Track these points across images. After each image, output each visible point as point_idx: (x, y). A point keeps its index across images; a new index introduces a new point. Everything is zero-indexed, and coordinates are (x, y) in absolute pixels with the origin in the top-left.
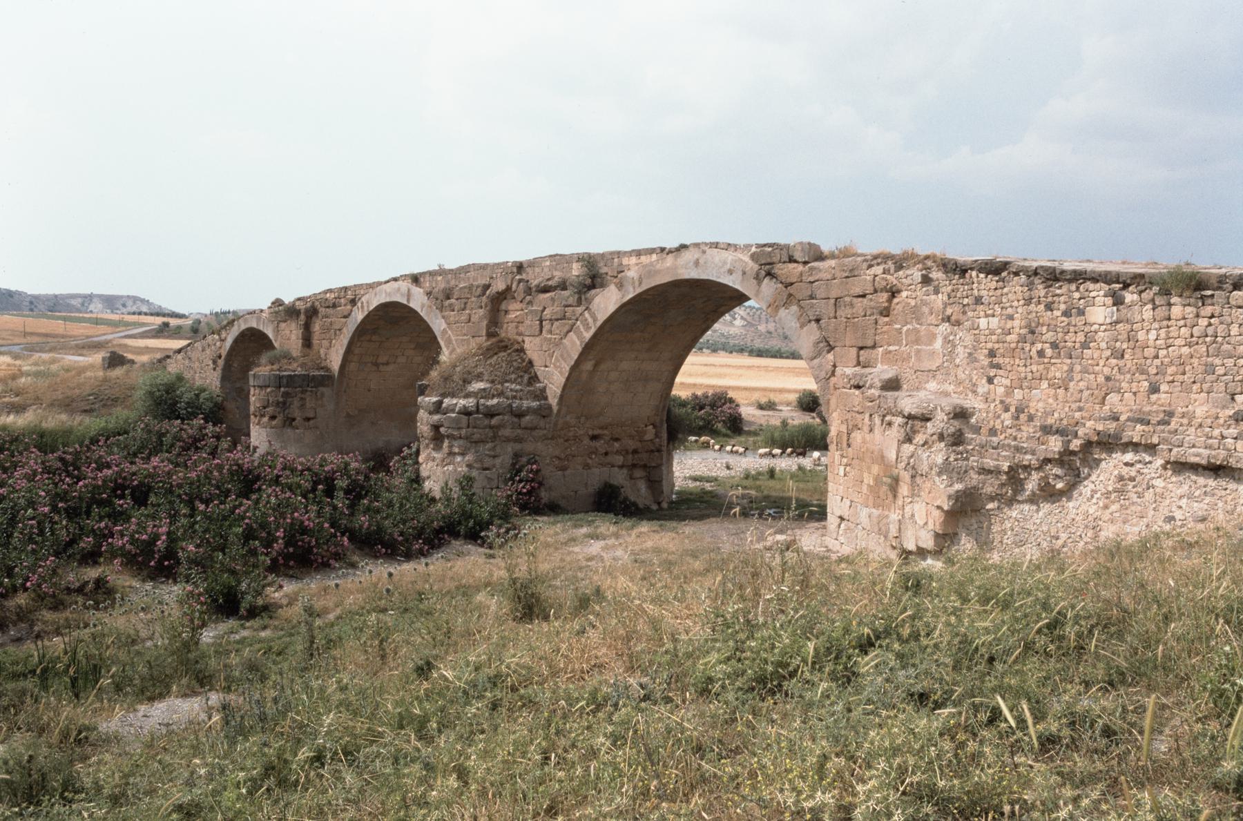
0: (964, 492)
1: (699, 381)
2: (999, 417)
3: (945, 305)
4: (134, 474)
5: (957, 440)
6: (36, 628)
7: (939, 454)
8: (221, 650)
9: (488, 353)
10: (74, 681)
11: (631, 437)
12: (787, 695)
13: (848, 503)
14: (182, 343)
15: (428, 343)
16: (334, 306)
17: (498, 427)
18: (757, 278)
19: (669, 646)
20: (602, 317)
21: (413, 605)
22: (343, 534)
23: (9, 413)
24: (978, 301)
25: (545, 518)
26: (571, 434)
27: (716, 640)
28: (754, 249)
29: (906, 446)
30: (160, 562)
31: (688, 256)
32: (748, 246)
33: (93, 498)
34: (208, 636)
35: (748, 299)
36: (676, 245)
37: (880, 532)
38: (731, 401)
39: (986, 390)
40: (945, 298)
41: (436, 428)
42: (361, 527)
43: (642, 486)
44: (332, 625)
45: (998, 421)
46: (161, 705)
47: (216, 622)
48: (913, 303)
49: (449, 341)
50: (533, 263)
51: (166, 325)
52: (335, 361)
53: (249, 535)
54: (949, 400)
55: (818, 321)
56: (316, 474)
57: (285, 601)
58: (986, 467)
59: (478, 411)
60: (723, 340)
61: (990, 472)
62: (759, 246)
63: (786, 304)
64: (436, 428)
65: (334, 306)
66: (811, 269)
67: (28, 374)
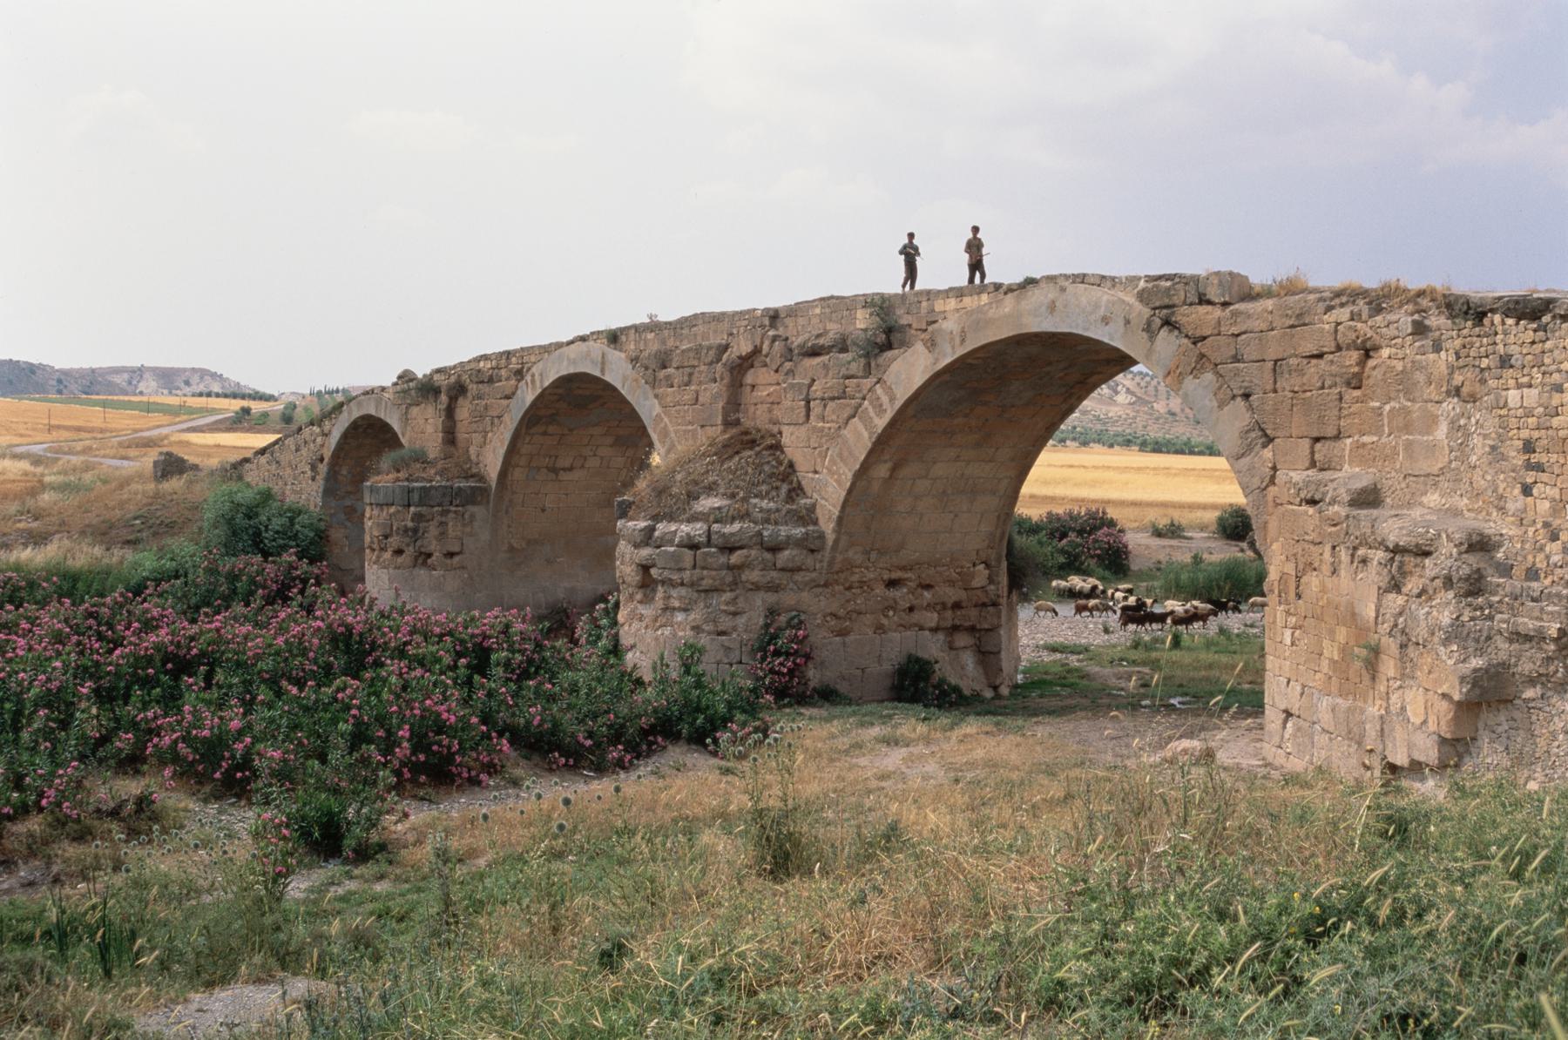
0: (1487, 671)
1: (1059, 491)
2: (1542, 549)
3: (1452, 370)
4: (192, 639)
5: (1474, 587)
6: (55, 869)
7: (1444, 610)
8: (315, 912)
9: (727, 450)
10: (104, 948)
11: (952, 583)
12: (1184, 1013)
13: (1299, 688)
14: (272, 438)
15: (632, 436)
16: (491, 380)
17: (739, 568)
18: (1148, 328)
19: (997, 927)
20: (903, 395)
21: (605, 848)
22: (501, 734)
23: (25, 545)
24: (1505, 362)
25: (814, 711)
26: (856, 578)
27: (1073, 920)
28: (1142, 284)
29: (1392, 596)
30: (229, 775)
31: (1037, 296)
32: (1133, 280)
33: (134, 674)
34: (298, 887)
35: (1135, 363)
36: (1019, 279)
37: (1349, 735)
38: (1111, 523)
39: (1519, 505)
40: (1452, 358)
41: (645, 568)
42: (528, 723)
43: (969, 660)
44: (482, 877)
45: (1540, 557)
46: (223, 995)
47: (310, 867)
48: (1399, 366)
49: (664, 434)
50: (795, 311)
51: (246, 411)
52: (492, 461)
53: (359, 738)
54: (1460, 522)
55: (1246, 396)
56: (462, 642)
57: (411, 837)
58: (1521, 629)
59: (709, 543)
60: (1099, 427)
61: (1528, 638)
62: (1150, 279)
63: (1195, 371)
64: (645, 568)
65: (491, 380)
66: (1235, 314)
67: (53, 487)
